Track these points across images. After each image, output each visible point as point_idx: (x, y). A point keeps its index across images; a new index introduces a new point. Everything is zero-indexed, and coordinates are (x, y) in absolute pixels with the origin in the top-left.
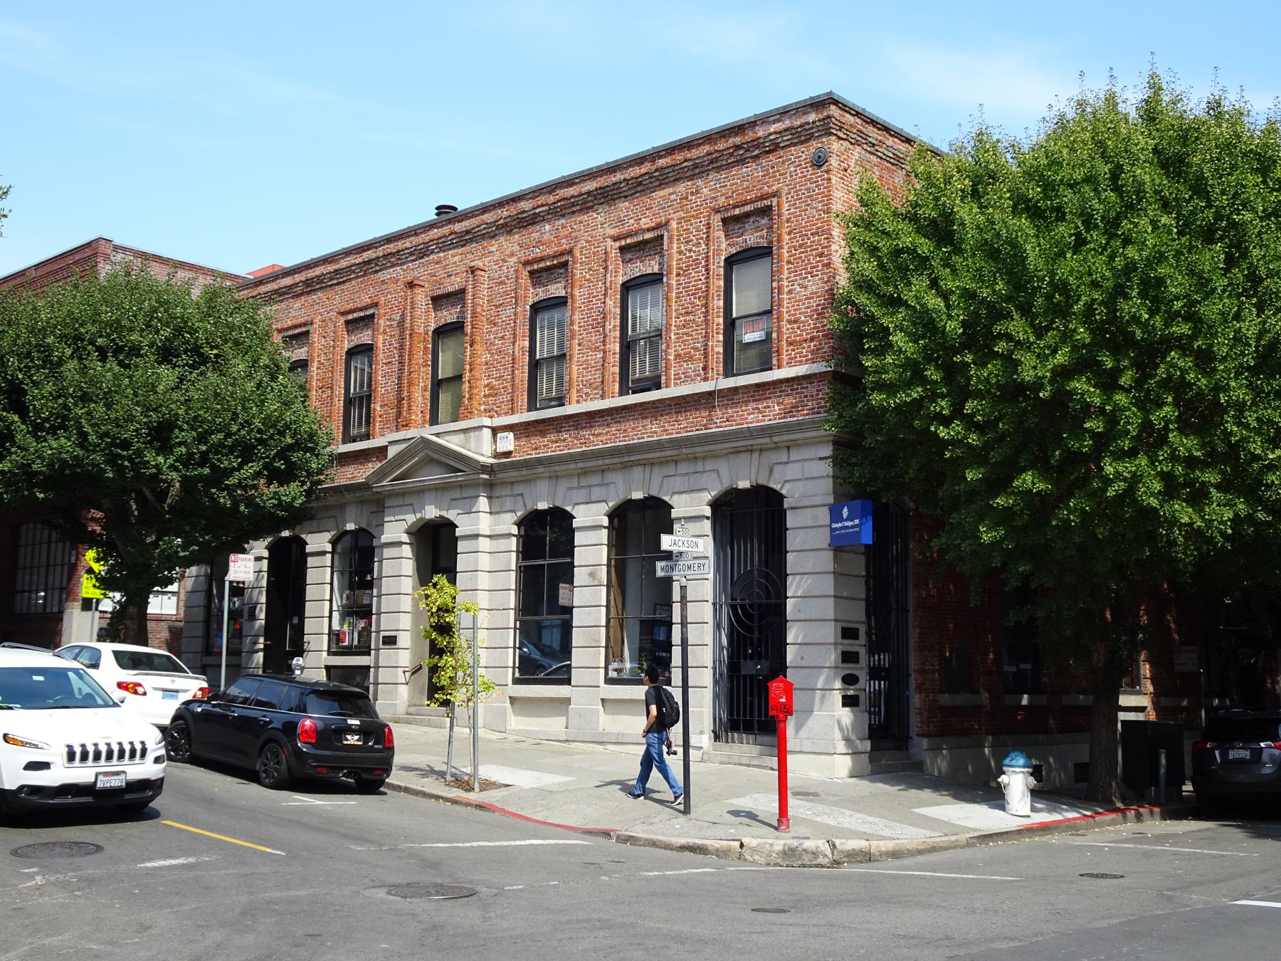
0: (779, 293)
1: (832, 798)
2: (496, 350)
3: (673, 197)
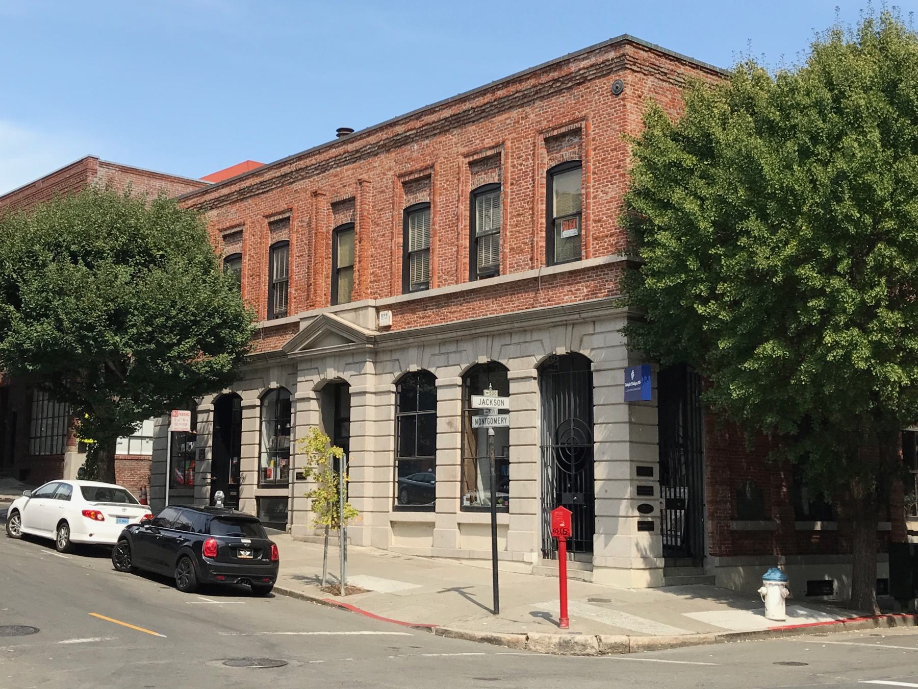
2: (379, 245)
3: (508, 121)
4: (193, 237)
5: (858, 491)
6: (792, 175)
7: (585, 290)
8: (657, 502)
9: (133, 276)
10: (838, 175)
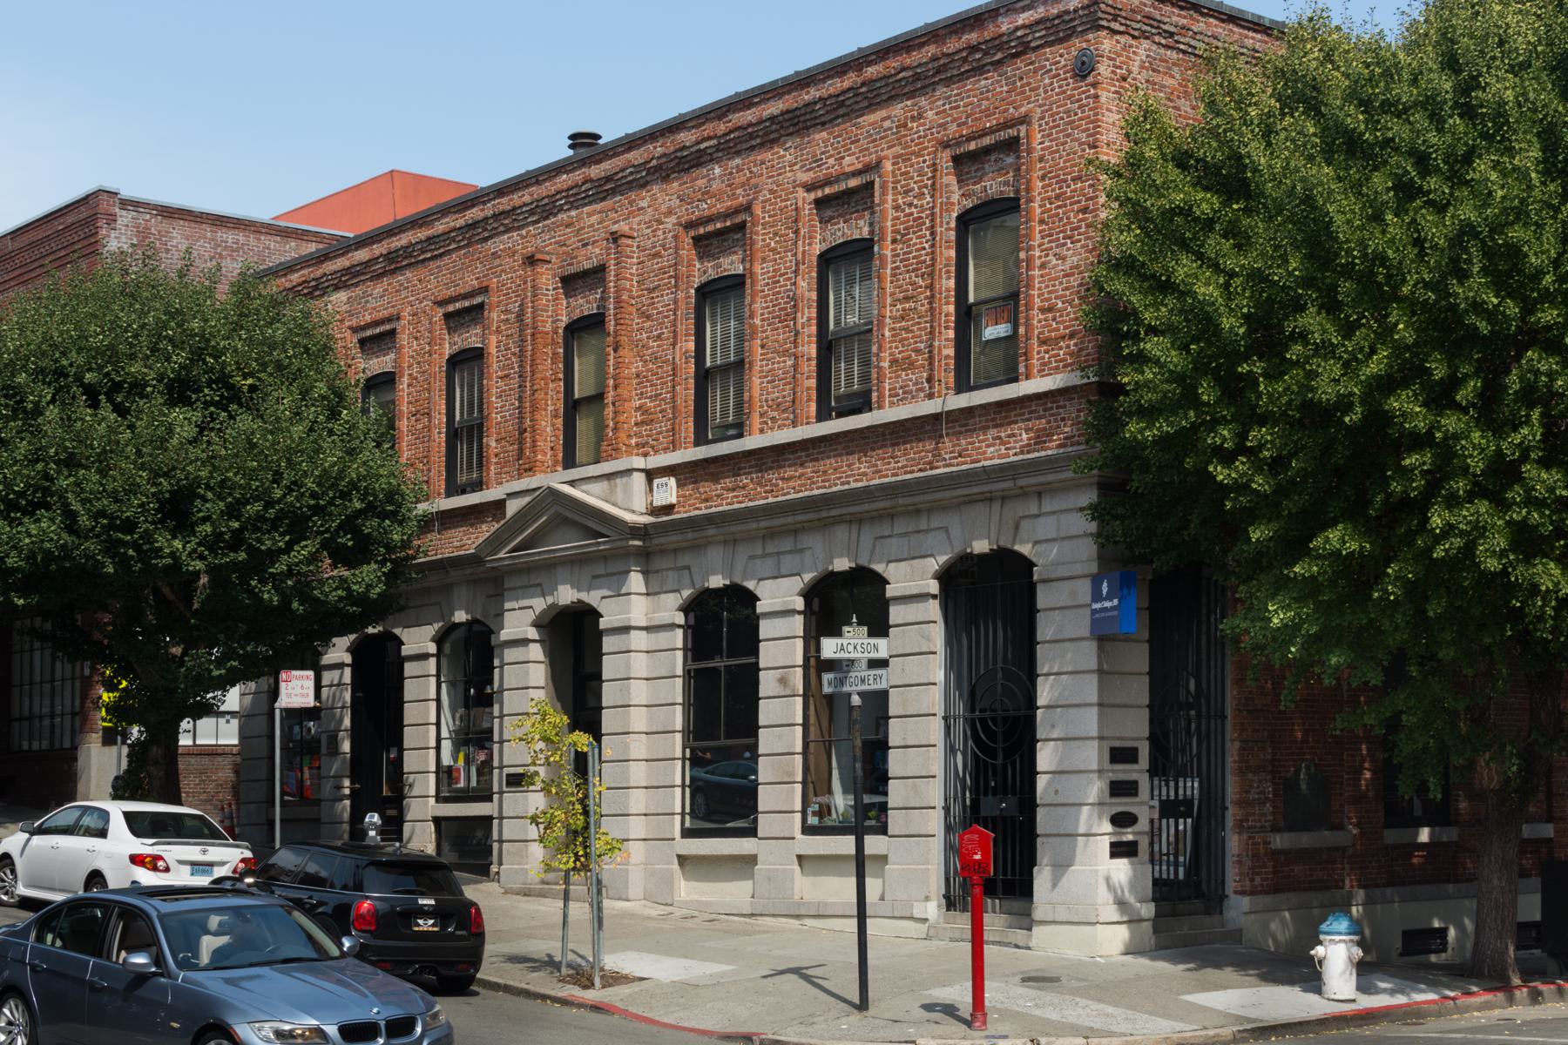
0: (1028, 269)
1: (1074, 984)
2: (652, 355)
3: (887, 124)
4: (307, 350)
5: (1489, 774)
6: (1384, 232)
7: (1025, 436)
8: (1144, 808)
9: (202, 429)
10: (1462, 233)
